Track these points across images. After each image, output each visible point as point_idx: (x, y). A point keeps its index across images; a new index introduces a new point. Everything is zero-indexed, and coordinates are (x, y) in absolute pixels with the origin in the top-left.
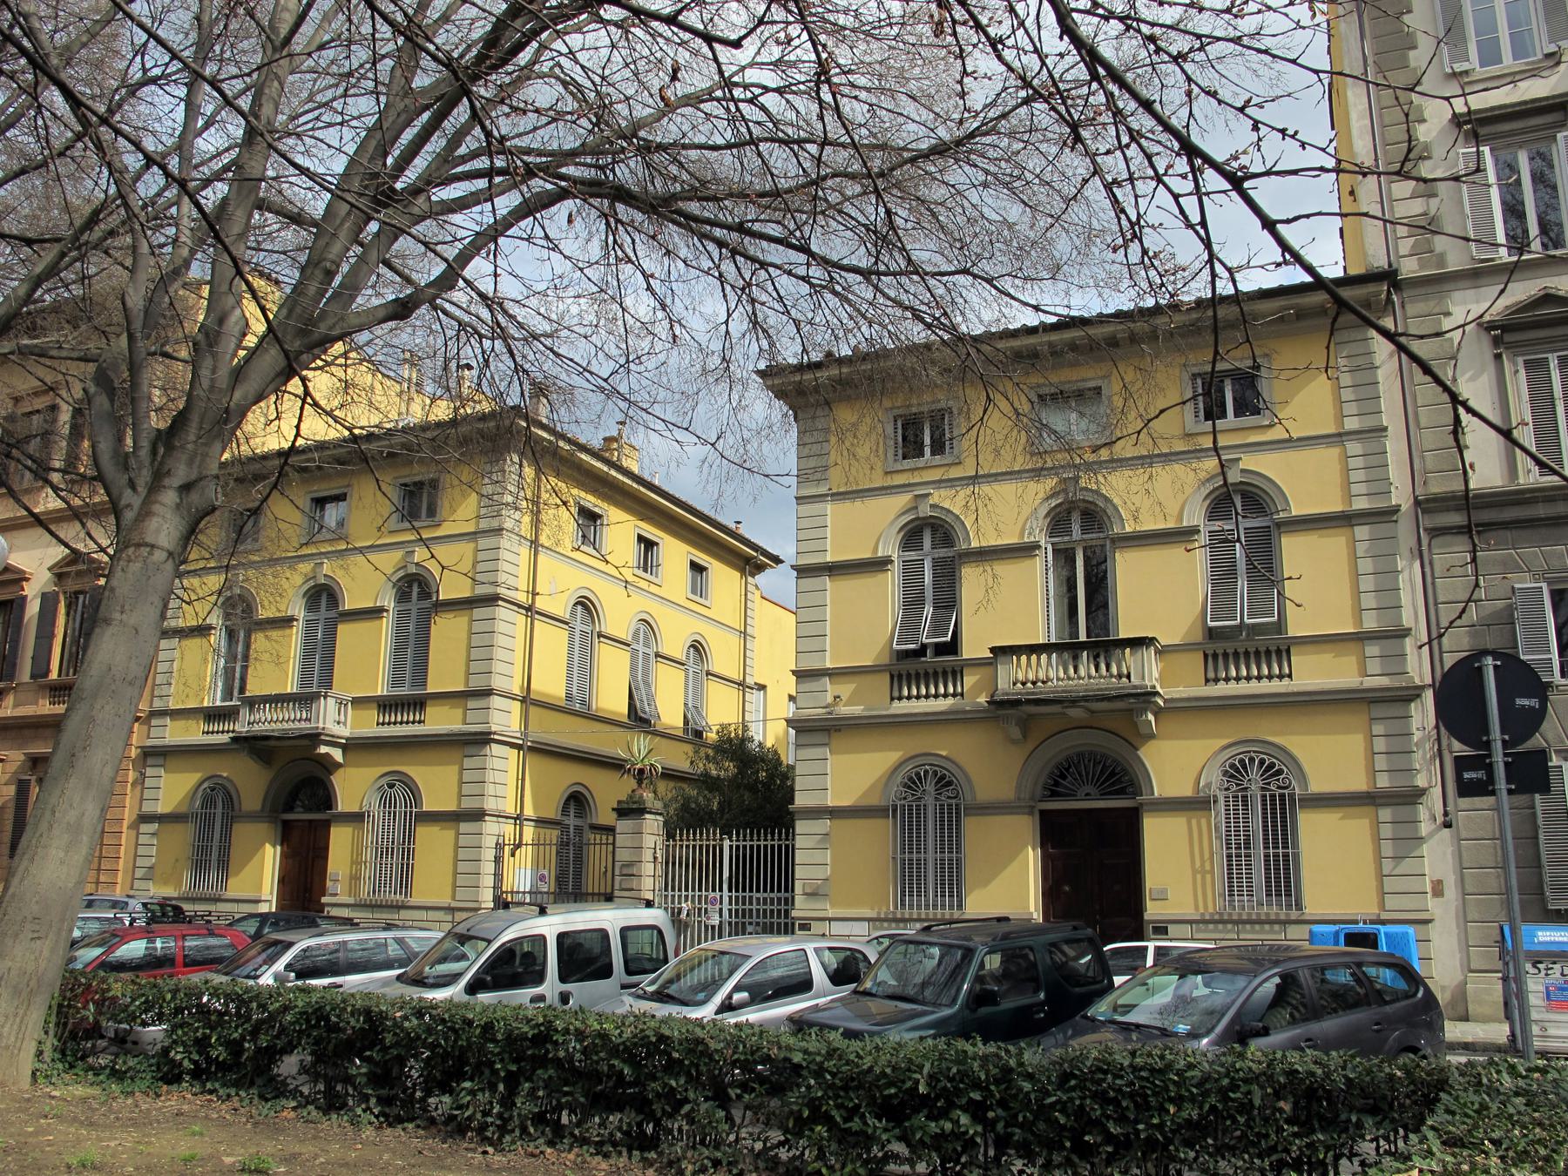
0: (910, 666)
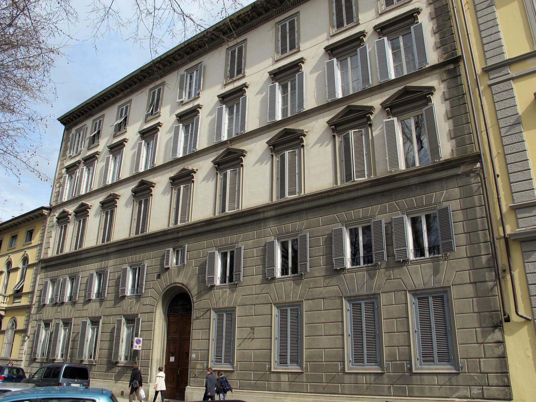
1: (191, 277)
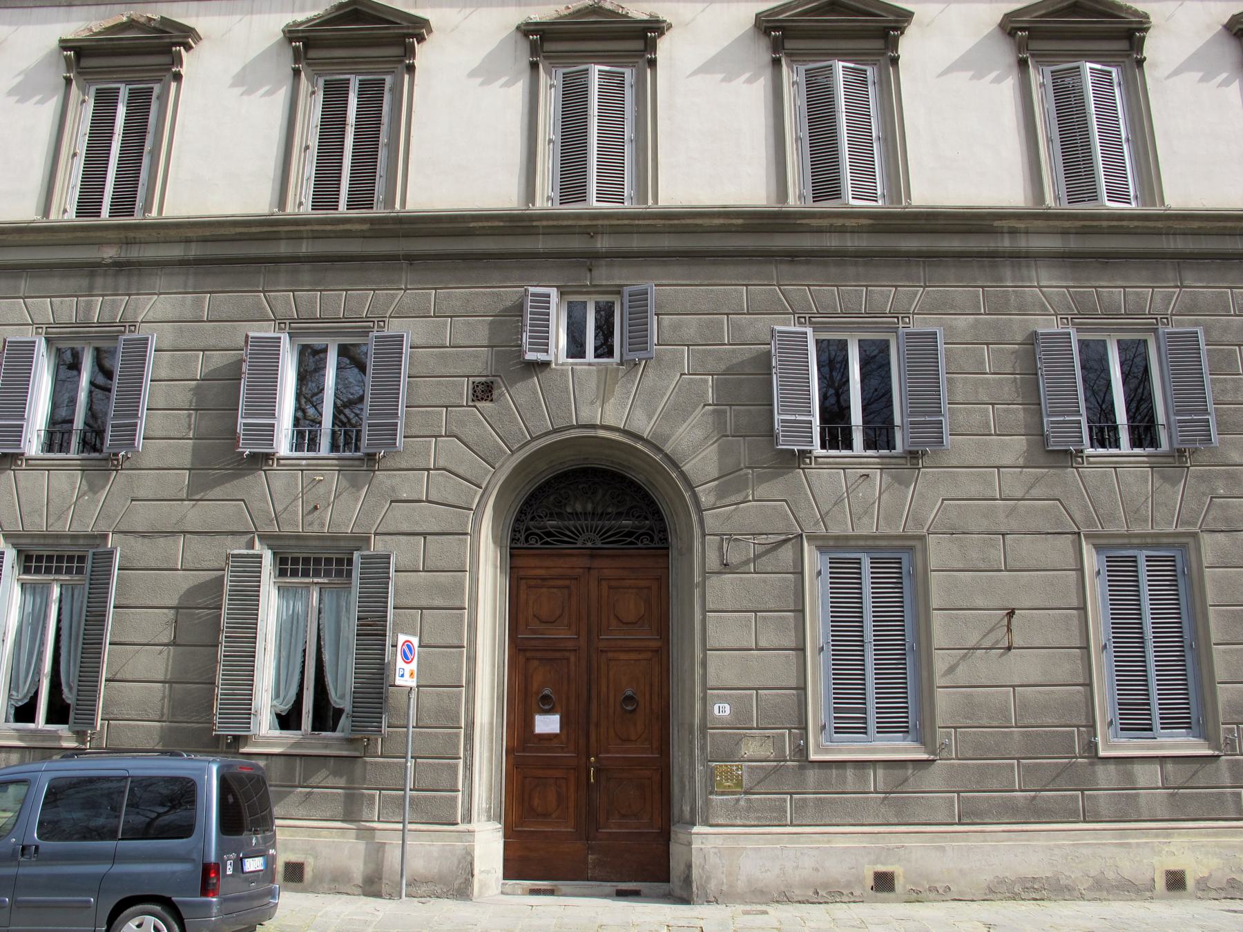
1: (678, 412)
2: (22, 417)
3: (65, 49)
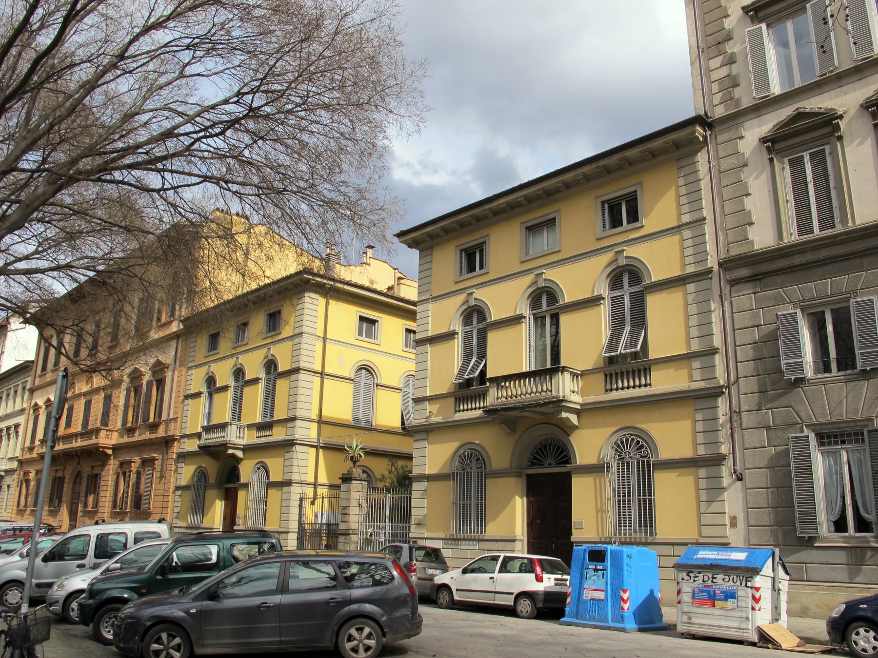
0: (465, 392)
2: (801, 357)
3: (764, 142)
